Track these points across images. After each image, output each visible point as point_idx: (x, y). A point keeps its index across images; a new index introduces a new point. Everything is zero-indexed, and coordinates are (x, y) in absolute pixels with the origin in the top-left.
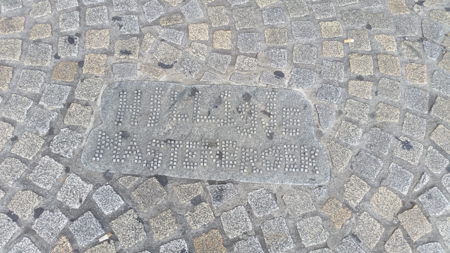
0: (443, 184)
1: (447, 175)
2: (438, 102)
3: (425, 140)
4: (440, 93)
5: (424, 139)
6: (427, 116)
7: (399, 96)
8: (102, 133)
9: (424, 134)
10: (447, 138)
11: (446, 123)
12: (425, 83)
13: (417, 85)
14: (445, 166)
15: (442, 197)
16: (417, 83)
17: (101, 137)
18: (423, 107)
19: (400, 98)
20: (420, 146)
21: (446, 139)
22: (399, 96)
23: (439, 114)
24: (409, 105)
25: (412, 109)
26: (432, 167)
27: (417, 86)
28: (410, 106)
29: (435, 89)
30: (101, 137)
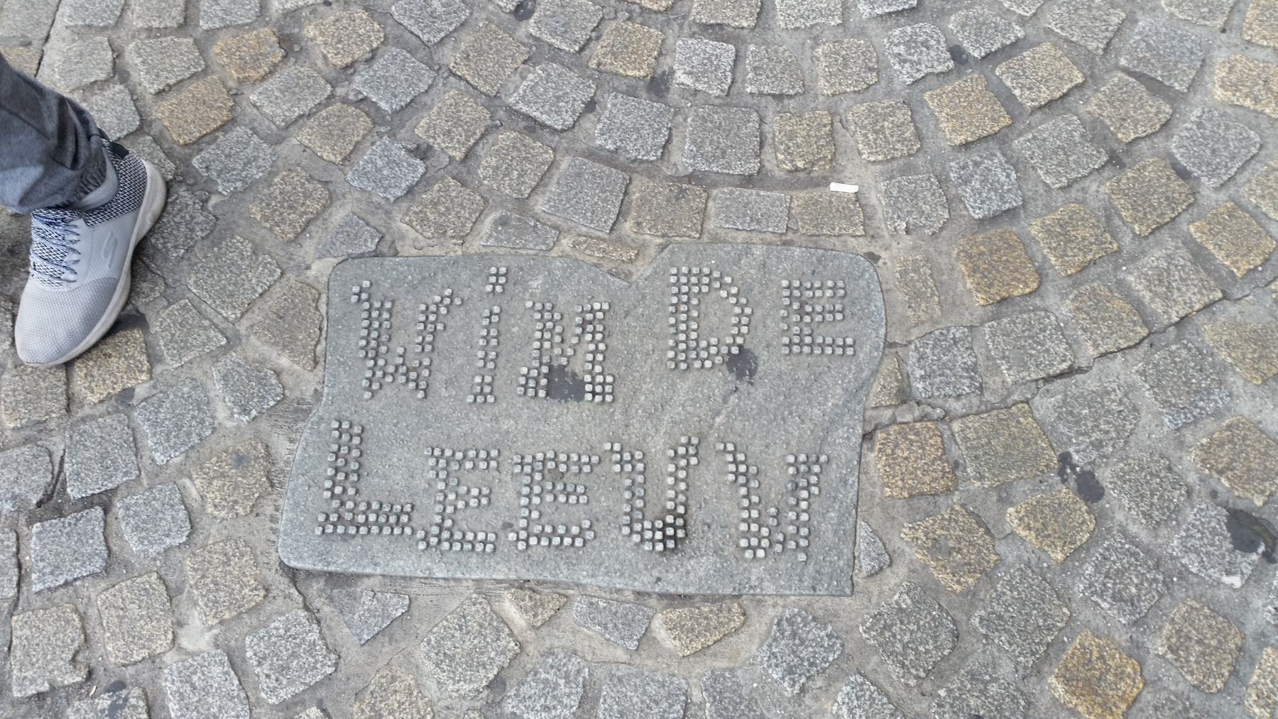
0: (921, 24)
1: (942, 40)
2: (1154, 102)
3: (1041, 31)
4: (1185, 122)
5: (1045, 28)
6: (1113, 62)
7: (1177, 14)
8: (602, 352)
9: (1059, 31)
10: (1043, 77)
11: (1088, 99)
12: (1219, 93)
13: (1213, 73)
14: (966, 45)
15: (889, 5)
16: (1221, 73)
17: (729, 452)
18: (1140, 60)
19: (1172, 14)
20: (1027, 9)
21: (1040, 74)
22: (1176, 11)
23: (1115, 88)
24: (1147, 28)
25: (1136, 30)
26: (967, 17)
27: (1206, 69)
28: (1144, 28)
29: (1197, 112)
30: (729, 452)
